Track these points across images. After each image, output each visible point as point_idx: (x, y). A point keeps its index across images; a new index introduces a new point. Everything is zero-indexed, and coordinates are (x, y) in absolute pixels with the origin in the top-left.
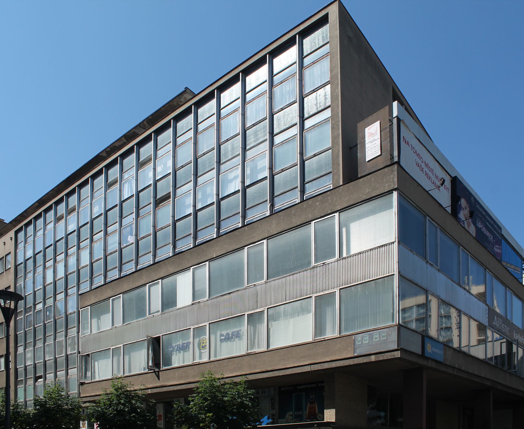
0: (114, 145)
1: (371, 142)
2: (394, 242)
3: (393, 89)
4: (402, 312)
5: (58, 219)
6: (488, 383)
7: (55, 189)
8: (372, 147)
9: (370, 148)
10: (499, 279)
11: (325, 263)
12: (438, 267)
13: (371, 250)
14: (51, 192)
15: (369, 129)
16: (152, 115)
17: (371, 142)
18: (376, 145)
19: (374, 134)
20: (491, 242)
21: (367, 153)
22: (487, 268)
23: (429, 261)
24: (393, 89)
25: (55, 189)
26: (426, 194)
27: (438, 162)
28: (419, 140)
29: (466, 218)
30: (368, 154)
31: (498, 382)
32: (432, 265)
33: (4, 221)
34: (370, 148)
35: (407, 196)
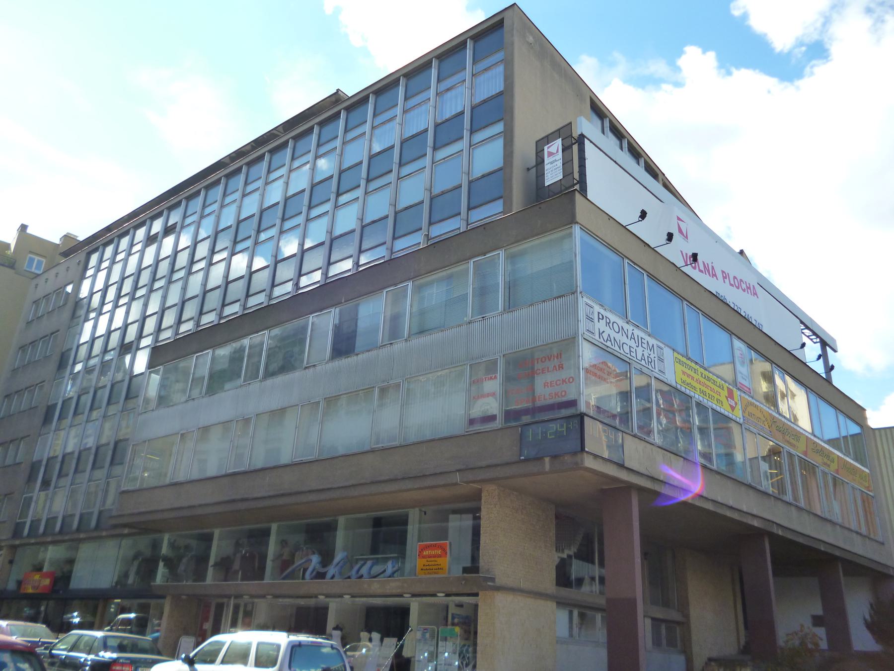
0: (272, 132)
1: (551, 163)
2: (575, 292)
3: (591, 100)
4: (665, 403)
5: (151, 240)
6: (756, 523)
7: (267, 134)
8: (552, 169)
9: (550, 171)
10: (759, 352)
11: (486, 317)
12: (648, 329)
13: (544, 301)
14: (307, 111)
15: (548, 148)
16: (172, 188)
17: (551, 163)
18: (557, 167)
19: (555, 154)
20: (88, 326)
21: (547, 176)
22: (732, 333)
23: (631, 321)
24: (591, 100)
25: (267, 134)
26: (624, 229)
27: (645, 188)
28: (615, 162)
29: (686, 262)
30: (548, 178)
31: (773, 522)
32: (638, 326)
33: (78, 239)
34: (550, 171)
35: (592, 233)
